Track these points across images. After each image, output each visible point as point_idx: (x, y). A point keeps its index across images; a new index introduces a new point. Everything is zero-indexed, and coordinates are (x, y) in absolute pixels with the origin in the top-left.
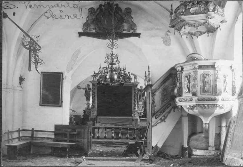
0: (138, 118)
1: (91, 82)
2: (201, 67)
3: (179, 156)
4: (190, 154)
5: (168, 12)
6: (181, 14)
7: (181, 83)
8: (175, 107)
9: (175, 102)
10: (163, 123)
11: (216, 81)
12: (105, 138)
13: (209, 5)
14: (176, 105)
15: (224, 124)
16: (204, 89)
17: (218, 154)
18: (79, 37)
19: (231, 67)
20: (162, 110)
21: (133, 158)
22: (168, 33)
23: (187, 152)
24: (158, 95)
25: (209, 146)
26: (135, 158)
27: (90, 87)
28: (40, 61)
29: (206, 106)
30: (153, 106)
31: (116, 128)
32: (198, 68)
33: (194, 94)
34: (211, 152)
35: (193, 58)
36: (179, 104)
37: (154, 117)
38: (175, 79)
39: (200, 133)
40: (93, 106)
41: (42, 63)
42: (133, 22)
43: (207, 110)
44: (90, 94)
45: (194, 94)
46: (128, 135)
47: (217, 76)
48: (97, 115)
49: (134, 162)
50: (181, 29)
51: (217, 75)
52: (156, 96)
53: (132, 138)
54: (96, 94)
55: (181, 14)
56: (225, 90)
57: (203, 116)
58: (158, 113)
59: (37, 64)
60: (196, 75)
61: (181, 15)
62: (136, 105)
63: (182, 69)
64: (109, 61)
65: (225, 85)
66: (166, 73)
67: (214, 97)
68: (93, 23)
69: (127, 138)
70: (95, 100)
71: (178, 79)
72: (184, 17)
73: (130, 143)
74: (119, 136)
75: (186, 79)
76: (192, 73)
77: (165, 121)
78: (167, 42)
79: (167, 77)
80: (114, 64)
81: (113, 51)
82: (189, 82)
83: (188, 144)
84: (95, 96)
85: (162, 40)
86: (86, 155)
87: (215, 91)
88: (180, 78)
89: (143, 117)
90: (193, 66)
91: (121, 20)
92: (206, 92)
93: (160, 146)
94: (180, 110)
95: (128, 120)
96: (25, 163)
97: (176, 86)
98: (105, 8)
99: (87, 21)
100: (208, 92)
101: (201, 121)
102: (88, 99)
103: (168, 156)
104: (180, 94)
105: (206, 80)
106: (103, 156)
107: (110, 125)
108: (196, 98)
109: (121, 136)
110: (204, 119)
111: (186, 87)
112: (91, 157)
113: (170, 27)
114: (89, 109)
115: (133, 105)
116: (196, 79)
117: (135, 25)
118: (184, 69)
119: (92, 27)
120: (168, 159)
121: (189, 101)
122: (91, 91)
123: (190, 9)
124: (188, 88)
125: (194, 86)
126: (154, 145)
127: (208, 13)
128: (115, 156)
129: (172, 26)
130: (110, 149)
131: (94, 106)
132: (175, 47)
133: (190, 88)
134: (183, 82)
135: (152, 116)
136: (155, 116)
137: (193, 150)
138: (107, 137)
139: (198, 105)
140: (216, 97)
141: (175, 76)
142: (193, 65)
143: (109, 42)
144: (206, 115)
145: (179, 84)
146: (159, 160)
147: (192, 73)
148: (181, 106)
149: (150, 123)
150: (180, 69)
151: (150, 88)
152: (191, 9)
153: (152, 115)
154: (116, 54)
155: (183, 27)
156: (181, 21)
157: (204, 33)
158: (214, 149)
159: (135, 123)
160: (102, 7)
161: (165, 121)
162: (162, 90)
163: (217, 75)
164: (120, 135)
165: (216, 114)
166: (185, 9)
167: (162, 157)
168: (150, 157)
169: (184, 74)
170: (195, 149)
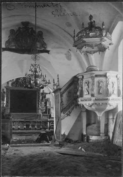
0: (41, 114)
1: (5, 87)
2: (96, 76)
3: (79, 141)
4: (88, 139)
5: (70, 36)
7: (82, 88)
8: (77, 105)
9: (77, 101)
10: (69, 116)
11: (107, 86)
12: (19, 129)
13: (103, 32)
15: (111, 117)
16: (99, 92)
17: (107, 138)
19: (117, 76)
20: (69, 107)
21: (45, 144)
22: (69, 51)
23: (86, 138)
24: (65, 95)
25: (101, 133)
26: (46, 143)
27: (4, 91)
29: (101, 104)
30: (62, 104)
31: (27, 122)
33: (93, 95)
34: (103, 138)
37: (63, 112)
39: (94, 123)
40: (7, 105)
42: (44, 42)
43: (102, 107)
44: (4, 96)
45: (93, 95)
46: (36, 127)
47: (108, 83)
49: (48, 147)
50: (82, 48)
51: (108, 82)
52: (63, 97)
53: (39, 129)
54: (9, 96)
56: (113, 93)
57: (98, 112)
58: (65, 110)
60: (94, 81)
62: (40, 104)
63: (83, 77)
64: (33, 70)
65: (113, 89)
66: (70, 81)
67: (106, 98)
69: (36, 129)
72: (85, 39)
73: (42, 132)
74: (30, 127)
75: (86, 84)
78: (69, 58)
80: (37, 72)
81: (35, 62)
83: (86, 133)
85: (65, 55)
86: (9, 143)
87: (107, 94)
89: (44, 113)
90: (91, 75)
92: (101, 94)
93: (66, 134)
95: (35, 115)
96: (50, 150)
99: (9, 40)
100: (102, 94)
103: (72, 141)
104: (81, 95)
105: (100, 85)
106: (21, 143)
107: (20, 119)
108: (94, 98)
110: (103, 114)
111: (86, 91)
112: (13, 144)
113: (73, 46)
115: (37, 105)
116: (93, 84)
117: (46, 44)
118: (84, 78)
119: (13, 44)
120: (72, 143)
121: (88, 100)
125: (92, 90)
126: (62, 133)
127: (102, 37)
128: (31, 143)
129: (75, 46)
130: (24, 138)
132: (74, 61)
134: (83, 86)
135: (61, 112)
137: (90, 136)
138: (20, 129)
139: (95, 103)
140: (108, 97)
144: (100, 110)
146: (67, 144)
149: (59, 117)
150: (81, 77)
151: (59, 91)
155: (83, 47)
156: (83, 42)
157: (97, 52)
158: (104, 135)
161: (70, 116)
162: (68, 92)
163: (108, 82)
164: (30, 127)
165: (107, 109)
167: (68, 142)
168: (59, 142)
170: (91, 135)
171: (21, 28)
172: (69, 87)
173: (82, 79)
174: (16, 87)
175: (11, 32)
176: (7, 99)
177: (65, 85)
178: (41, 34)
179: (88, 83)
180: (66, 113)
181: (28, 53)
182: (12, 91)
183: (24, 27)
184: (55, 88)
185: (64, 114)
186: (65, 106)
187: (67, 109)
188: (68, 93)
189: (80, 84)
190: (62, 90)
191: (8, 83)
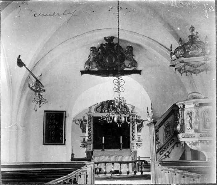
6: (181, 56)
7: (183, 120)
8: (178, 143)
9: (178, 138)
14: (179, 140)
18: (81, 71)
27: (85, 119)
28: (44, 100)
29: (208, 142)
30: (157, 142)
32: (198, 106)
35: (194, 97)
36: (181, 140)
38: (177, 115)
41: (45, 102)
48: (94, 149)
54: (92, 126)
55: (181, 56)
58: (161, 150)
59: (41, 103)
61: (181, 57)
63: (184, 106)
68: (94, 61)
70: (91, 132)
71: (180, 116)
75: (188, 116)
76: (194, 111)
77: (169, 157)
81: (119, 95)
82: (191, 119)
84: (92, 128)
88: (182, 115)
91: (123, 59)
94: (183, 146)
97: (178, 123)
98: (106, 47)
99: (89, 60)
101: (204, 155)
102: (84, 131)
104: (183, 131)
109: (99, 171)
114: (85, 142)
118: (185, 107)
119: (95, 65)
121: (192, 137)
122: (87, 123)
123: (188, 52)
124: (190, 124)
131: (90, 139)
133: (192, 125)
136: (159, 153)
139: (201, 141)
141: (177, 112)
142: (194, 103)
143: (115, 87)
145: (182, 120)
147: (194, 111)
148: (185, 142)
150: (182, 106)
152: (190, 52)
153: (156, 152)
154: (123, 97)
159: (134, 156)
160: (104, 46)
166: (185, 51)
169: (185, 112)
171: (104, 45)
173: (183, 109)
174: (101, 113)
175: (91, 50)
176: (89, 130)
177: (164, 115)
178: (130, 49)
179: (190, 114)
180: (164, 153)
181: (114, 76)
182: (96, 119)
183: (107, 43)
185: (161, 155)
186: (162, 143)
187: (164, 149)
188: (166, 127)
189: (181, 115)
190: (157, 123)
191: (90, 108)
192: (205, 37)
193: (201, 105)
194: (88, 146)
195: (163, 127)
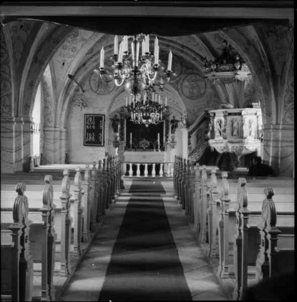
7: (213, 127)
33: (225, 138)
63: (215, 114)
76: (223, 119)
79: (200, 122)
82: (221, 127)
104: (213, 137)
118: (216, 115)
125: (224, 131)
134: (215, 125)
169: (216, 120)
172: (199, 126)
184: (195, 91)
186: (193, 148)
192: (109, 44)
193: (230, 114)
194: (120, 146)
195: (195, 133)
